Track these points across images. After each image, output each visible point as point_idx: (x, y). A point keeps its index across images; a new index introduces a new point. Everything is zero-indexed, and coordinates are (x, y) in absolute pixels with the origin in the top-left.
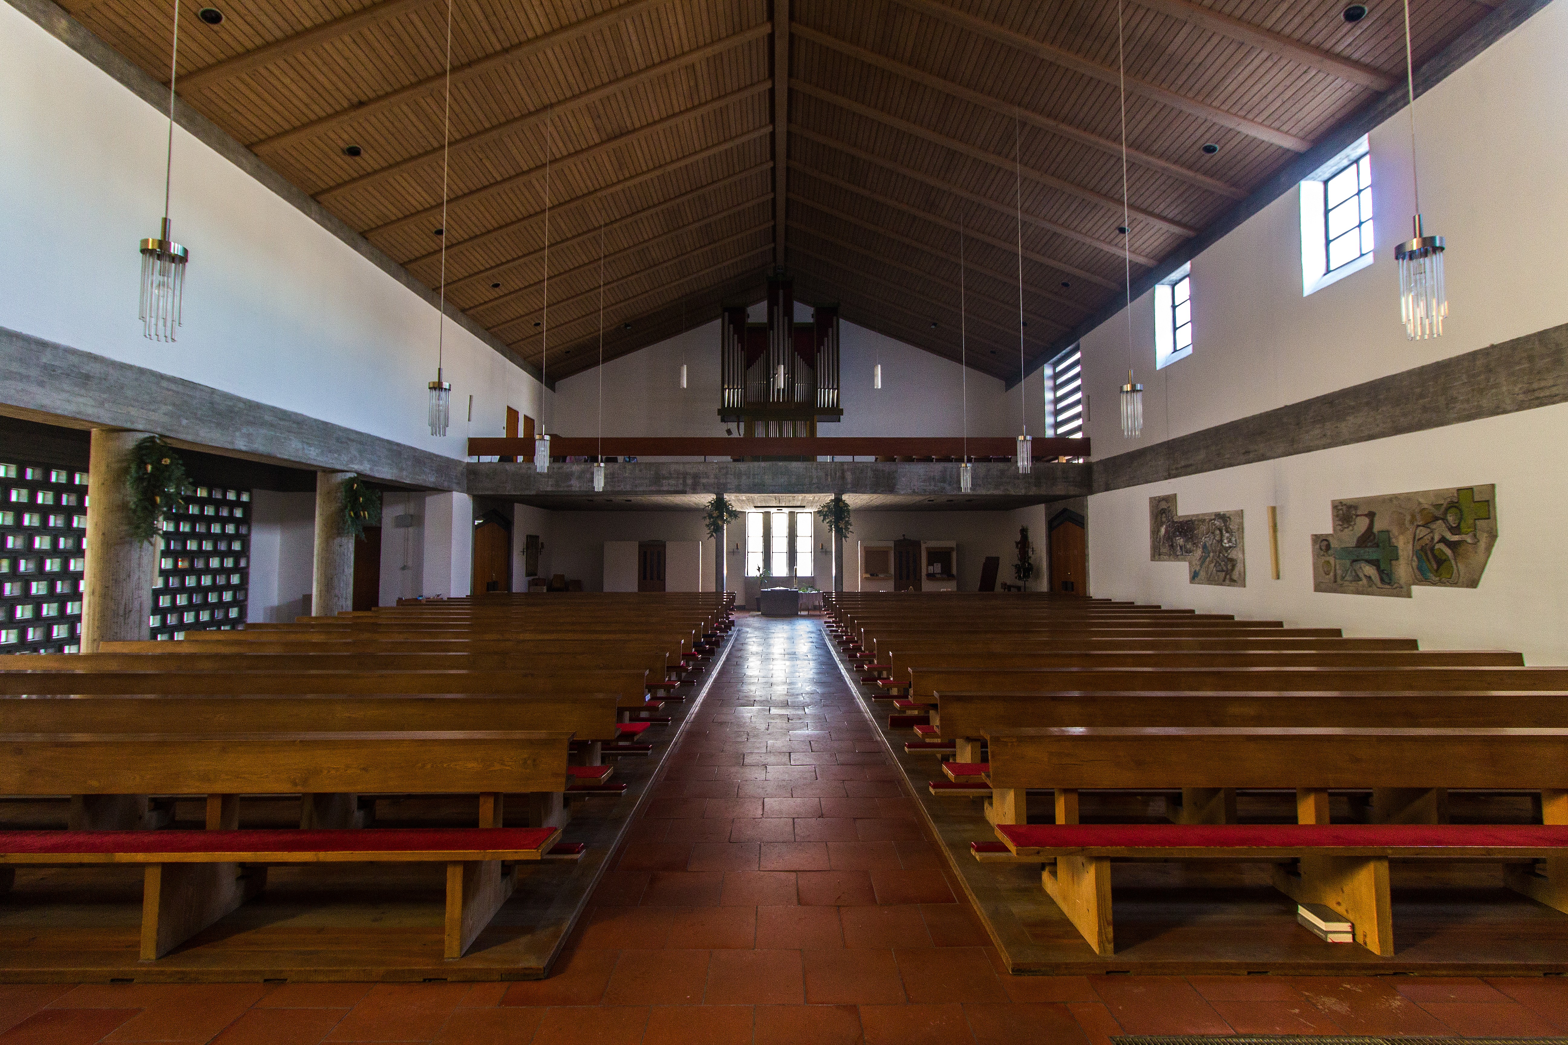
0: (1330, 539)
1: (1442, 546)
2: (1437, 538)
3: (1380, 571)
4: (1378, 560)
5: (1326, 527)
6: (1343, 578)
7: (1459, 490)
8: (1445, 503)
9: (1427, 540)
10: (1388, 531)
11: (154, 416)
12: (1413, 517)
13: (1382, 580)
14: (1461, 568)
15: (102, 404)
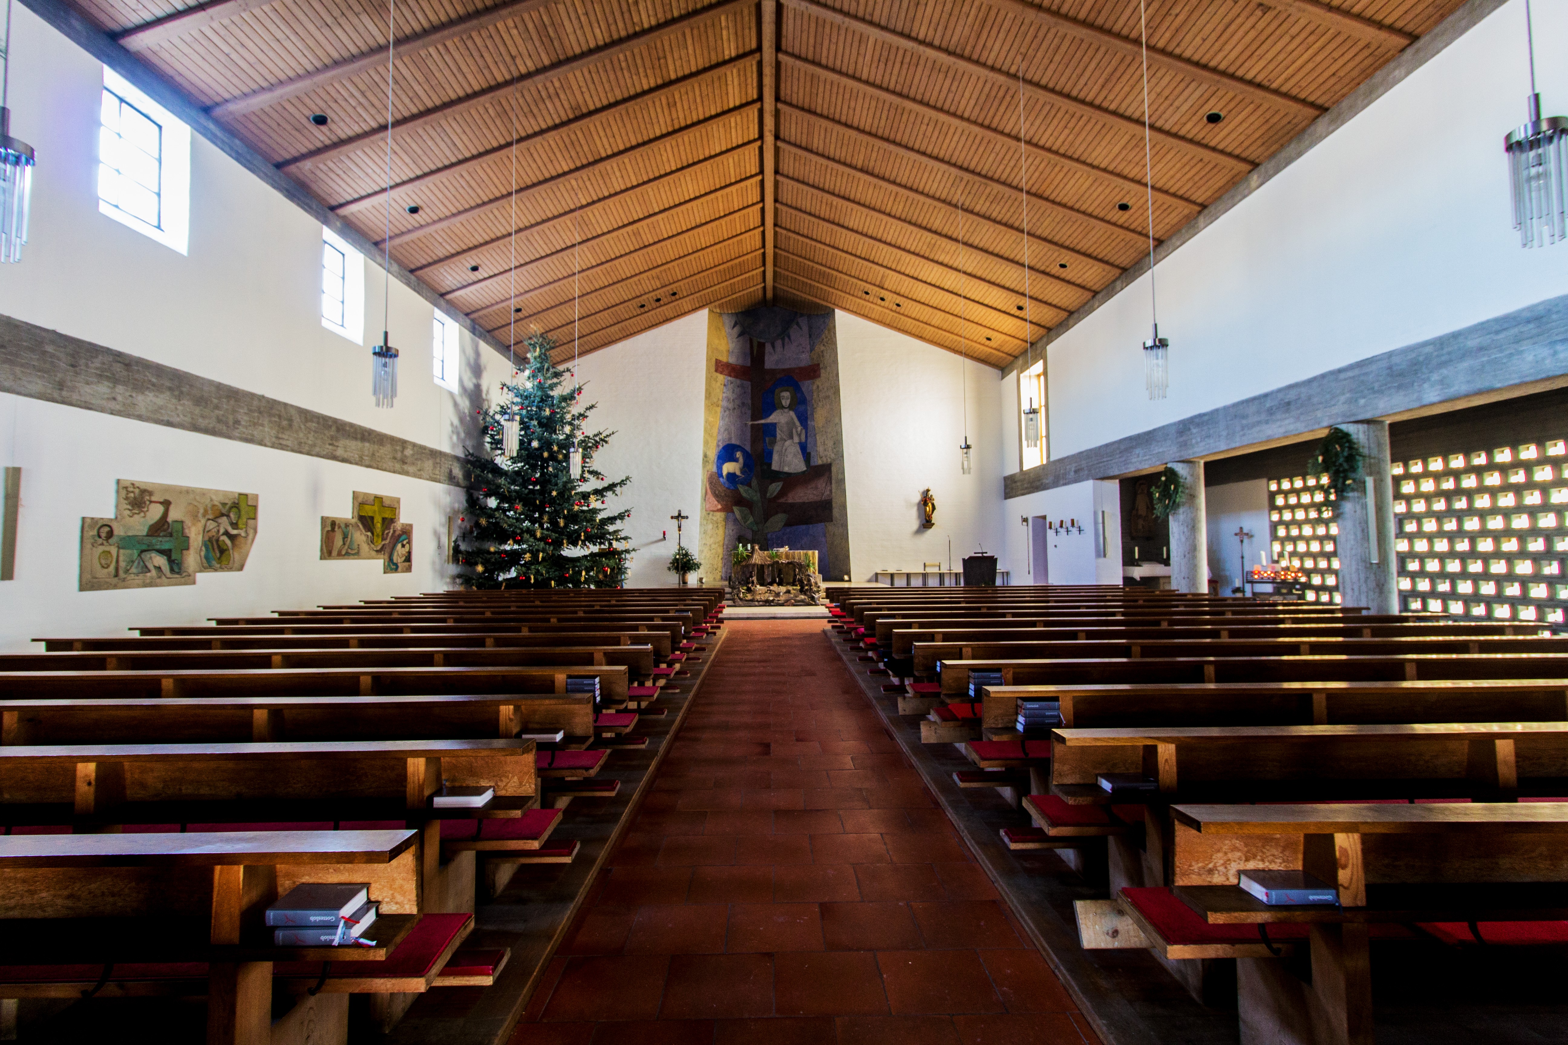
0: (115, 526)
1: (225, 538)
2: (222, 531)
3: (171, 561)
4: (170, 550)
5: (106, 508)
6: (127, 571)
7: (240, 494)
8: (230, 503)
9: (213, 533)
10: (182, 522)
11: (1335, 410)
12: (206, 511)
13: (172, 570)
14: (236, 556)
15: (1298, 419)
